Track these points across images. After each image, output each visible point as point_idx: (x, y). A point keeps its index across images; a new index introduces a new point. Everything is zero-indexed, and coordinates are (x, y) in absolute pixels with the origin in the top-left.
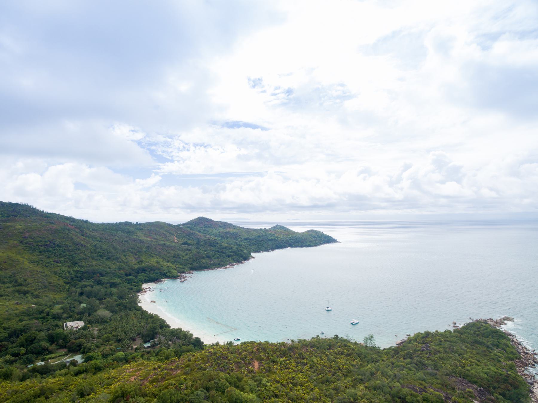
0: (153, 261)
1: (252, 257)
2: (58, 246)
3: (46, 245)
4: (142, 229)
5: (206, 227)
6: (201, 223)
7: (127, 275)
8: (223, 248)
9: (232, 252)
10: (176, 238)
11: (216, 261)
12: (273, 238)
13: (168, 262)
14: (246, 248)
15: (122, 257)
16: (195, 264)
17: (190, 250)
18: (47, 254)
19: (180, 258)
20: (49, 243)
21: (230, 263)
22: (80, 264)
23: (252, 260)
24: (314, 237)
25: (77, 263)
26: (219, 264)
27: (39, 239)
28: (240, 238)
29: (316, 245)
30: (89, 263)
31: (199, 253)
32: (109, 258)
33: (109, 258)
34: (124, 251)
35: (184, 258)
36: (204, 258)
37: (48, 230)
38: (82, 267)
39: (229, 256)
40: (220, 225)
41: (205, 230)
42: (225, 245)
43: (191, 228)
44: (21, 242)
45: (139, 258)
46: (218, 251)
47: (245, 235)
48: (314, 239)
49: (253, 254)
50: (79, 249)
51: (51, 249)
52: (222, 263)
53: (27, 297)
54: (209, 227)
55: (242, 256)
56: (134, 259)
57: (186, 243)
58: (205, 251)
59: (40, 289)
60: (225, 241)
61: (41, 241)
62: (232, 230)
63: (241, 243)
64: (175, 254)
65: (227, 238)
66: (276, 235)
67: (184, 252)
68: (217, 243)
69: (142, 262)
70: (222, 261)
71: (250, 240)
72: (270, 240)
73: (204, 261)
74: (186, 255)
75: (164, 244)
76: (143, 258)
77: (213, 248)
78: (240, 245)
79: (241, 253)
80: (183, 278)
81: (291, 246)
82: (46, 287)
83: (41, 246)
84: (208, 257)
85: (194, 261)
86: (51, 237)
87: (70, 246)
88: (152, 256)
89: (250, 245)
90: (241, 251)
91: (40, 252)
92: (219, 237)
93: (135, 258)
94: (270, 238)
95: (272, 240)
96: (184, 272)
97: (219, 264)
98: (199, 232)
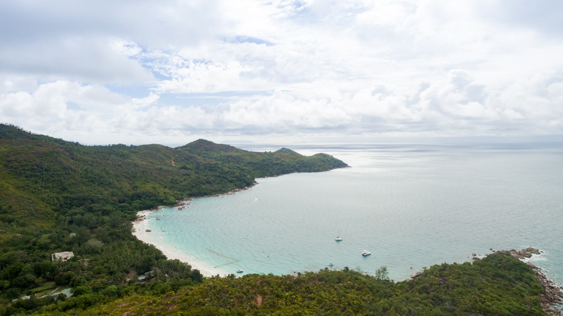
0: (149, 187)
1: (256, 182)
2: (46, 170)
3: (33, 169)
4: (137, 152)
5: (207, 150)
6: (201, 146)
7: (120, 202)
8: (225, 173)
9: (234, 177)
10: (173, 162)
11: (216, 187)
12: (278, 162)
13: (165, 187)
14: (250, 172)
15: (115, 182)
16: (194, 190)
17: (189, 175)
18: (33, 179)
19: (178, 183)
20: (36, 167)
21: (233, 189)
22: (69, 190)
23: (256, 186)
24: (323, 161)
25: (66, 189)
26: (220, 190)
27: (25, 163)
28: (243, 162)
29: (325, 169)
30: (79, 189)
31: (198, 178)
32: (101, 183)
33: (101, 183)
34: (117, 176)
35: (182, 184)
36: (204, 184)
37: (35, 153)
38: (72, 193)
39: (231, 182)
40: (222, 148)
41: (205, 153)
42: (226, 169)
43: (190, 151)
44: (6, 166)
45: (133, 183)
46: (219, 177)
47: (248, 159)
48: (324, 163)
49: (256, 180)
50: (69, 174)
51: (39, 174)
52: (224, 189)
53: (12, 226)
54: (210, 150)
55: (245, 182)
56: (128, 185)
57: (184, 168)
58: (205, 176)
59: (26, 217)
60: (227, 165)
61: (27, 165)
62: (234, 154)
63: (244, 167)
64: (172, 180)
65: (229, 162)
66: (282, 159)
67: (182, 177)
68: (218, 168)
69: (136, 187)
70: (223, 187)
71: (254, 164)
72: (275, 164)
73: (204, 187)
74: (185, 180)
75: (161, 168)
76: (138, 184)
77: (213, 173)
78: (242, 170)
79: (243, 178)
80: (182, 205)
81: (299, 171)
82: (32, 215)
83: (28, 170)
84: (208, 182)
85: (193, 187)
86: (38, 161)
87: (59, 171)
88: (148, 182)
89: (254, 170)
90: (244, 176)
91: (27, 177)
92: (220, 160)
93: (129, 183)
94: (275, 162)
95: (277, 164)
96: (182, 199)
97: (220, 190)
98: (199, 155)
